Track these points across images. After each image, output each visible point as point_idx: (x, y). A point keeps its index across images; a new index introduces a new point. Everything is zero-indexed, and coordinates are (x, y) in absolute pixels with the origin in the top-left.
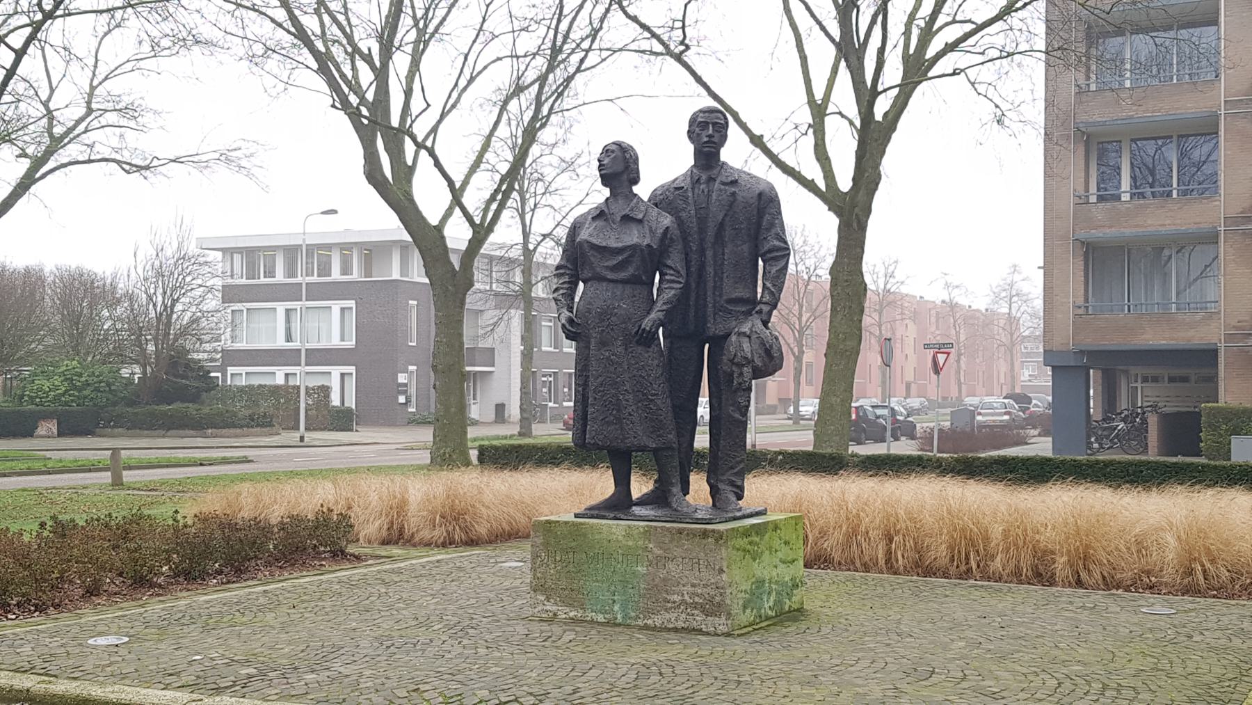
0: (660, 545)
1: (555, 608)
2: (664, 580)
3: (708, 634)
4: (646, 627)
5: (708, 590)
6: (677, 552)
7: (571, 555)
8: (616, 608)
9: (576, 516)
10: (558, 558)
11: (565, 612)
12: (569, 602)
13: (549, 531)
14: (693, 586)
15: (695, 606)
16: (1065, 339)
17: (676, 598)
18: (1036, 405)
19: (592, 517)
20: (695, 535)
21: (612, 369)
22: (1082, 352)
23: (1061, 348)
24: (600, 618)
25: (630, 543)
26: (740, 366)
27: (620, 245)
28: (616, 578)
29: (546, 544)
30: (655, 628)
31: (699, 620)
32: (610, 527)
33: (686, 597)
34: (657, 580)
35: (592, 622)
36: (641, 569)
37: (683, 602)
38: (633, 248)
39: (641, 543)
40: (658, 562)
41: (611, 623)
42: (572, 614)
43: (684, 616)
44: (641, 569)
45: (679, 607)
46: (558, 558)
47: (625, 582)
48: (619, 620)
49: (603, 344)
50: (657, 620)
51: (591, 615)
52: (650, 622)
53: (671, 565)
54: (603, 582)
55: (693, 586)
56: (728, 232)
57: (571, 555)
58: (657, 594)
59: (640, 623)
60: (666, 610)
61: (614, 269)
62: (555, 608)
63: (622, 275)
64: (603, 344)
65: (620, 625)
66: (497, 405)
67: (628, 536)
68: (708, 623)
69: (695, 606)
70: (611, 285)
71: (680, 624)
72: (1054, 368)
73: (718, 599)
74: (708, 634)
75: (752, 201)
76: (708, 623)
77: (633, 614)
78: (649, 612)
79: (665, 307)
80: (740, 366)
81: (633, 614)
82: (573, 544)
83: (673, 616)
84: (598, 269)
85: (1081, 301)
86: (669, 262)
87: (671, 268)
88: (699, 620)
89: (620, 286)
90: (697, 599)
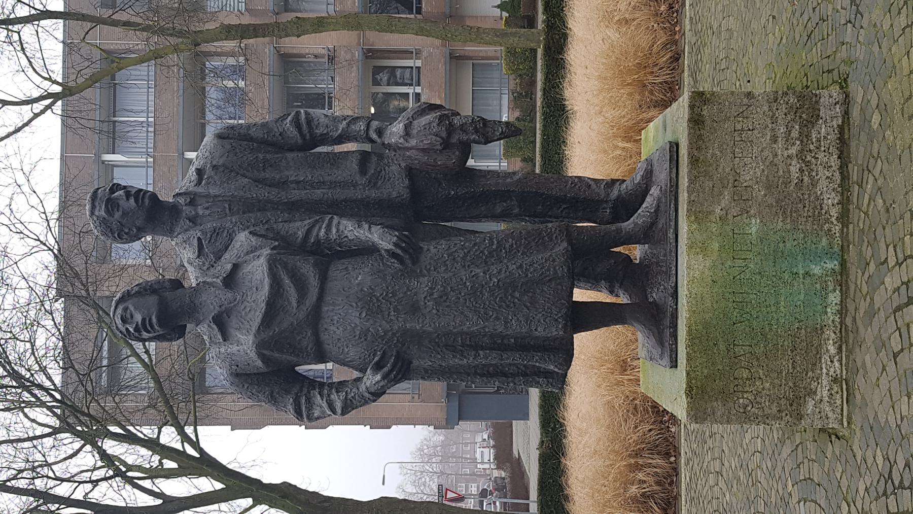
2: (769, 187)
3: (846, 114)
4: (844, 218)
5: (780, 114)
6: (725, 166)
8: (816, 270)
9: (674, 364)
10: (745, 374)
11: (830, 366)
12: (813, 356)
14: (774, 139)
15: (805, 137)
16: (438, 409)
17: (794, 169)
18: (489, 486)
19: (675, 336)
20: (700, 137)
21: (452, 296)
22: (448, 395)
23: (445, 414)
24: (834, 298)
25: (716, 246)
26: (451, 130)
27: (267, 282)
29: (725, 395)
30: (845, 203)
32: (691, 281)
33: (793, 151)
34: (771, 200)
35: (842, 311)
37: (800, 156)
38: (272, 265)
39: (714, 228)
40: (741, 198)
41: (842, 276)
42: (832, 350)
43: (821, 155)
44: (754, 227)
45: (808, 164)
49: (415, 309)
50: (831, 199)
51: (831, 316)
52: (834, 212)
53: (746, 177)
54: (778, 294)
55: (774, 139)
56: (269, 174)
59: (837, 228)
61: (302, 289)
63: (313, 282)
64: (415, 309)
65: (843, 264)
69: (805, 137)
70: (328, 298)
71: (834, 162)
72: (459, 419)
73: (792, 100)
74: (846, 114)
75: (228, 147)
77: (824, 241)
78: (818, 215)
79: (366, 226)
80: (451, 130)
81: (824, 241)
82: (722, 347)
83: (823, 174)
84: (301, 316)
85: (409, 397)
86: (300, 234)
87: (309, 232)
89: (330, 285)
90: (795, 134)
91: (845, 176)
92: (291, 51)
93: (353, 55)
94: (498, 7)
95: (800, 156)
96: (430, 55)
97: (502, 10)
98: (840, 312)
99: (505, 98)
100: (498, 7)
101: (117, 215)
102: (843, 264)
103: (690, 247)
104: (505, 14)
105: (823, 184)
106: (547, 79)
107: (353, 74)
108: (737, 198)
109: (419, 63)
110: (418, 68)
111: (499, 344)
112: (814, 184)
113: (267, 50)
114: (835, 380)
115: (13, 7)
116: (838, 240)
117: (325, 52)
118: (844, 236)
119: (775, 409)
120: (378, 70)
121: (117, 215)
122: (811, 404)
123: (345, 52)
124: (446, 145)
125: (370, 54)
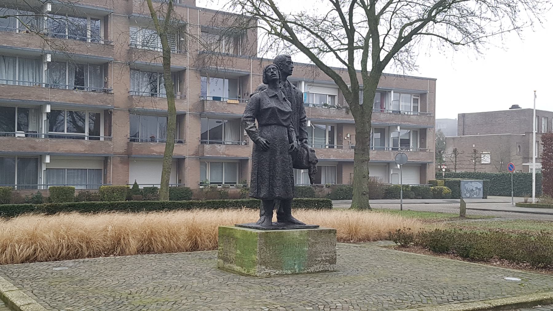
2: (315, 252)
4: (308, 273)
6: (320, 240)
10: (271, 248)
11: (273, 272)
17: (319, 259)
24: (289, 272)
29: (266, 242)
30: (312, 273)
31: (328, 266)
33: (323, 258)
37: (322, 260)
40: (313, 245)
42: (277, 273)
47: (299, 255)
48: (297, 271)
50: (312, 269)
53: (317, 245)
58: (312, 259)
59: (305, 271)
61: (285, 121)
65: (297, 274)
67: (301, 235)
71: (321, 269)
78: (310, 266)
83: (318, 266)
88: (328, 266)
90: (327, 258)
91: (318, 272)
92: (109, 69)
93: (109, 104)
94: (136, 183)
95: (322, 260)
96: (110, 146)
97: (134, 185)
98: (286, 274)
99: (83, 188)
100: (136, 183)
101: (287, 64)
102: (297, 274)
103: (301, 231)
104: (131, 187)
105: (316, 267)
106: (184, 204)
107: (98, 103)
108: (313, 243)
109: (102, 139)
110: (99, 139)
111: (272, 178)
112: (316, 264)
113: (111, 57)
114: (270, 274)
115: (340, 41)
116: (303, 272)
117: (109, 88)
118: (304, 273)
119: (262, 257)
120: (98, 116)
121: (287, 64)
122: (264, 267)
123: (110, 100)
124: (309, 163)
125: (108, 114)
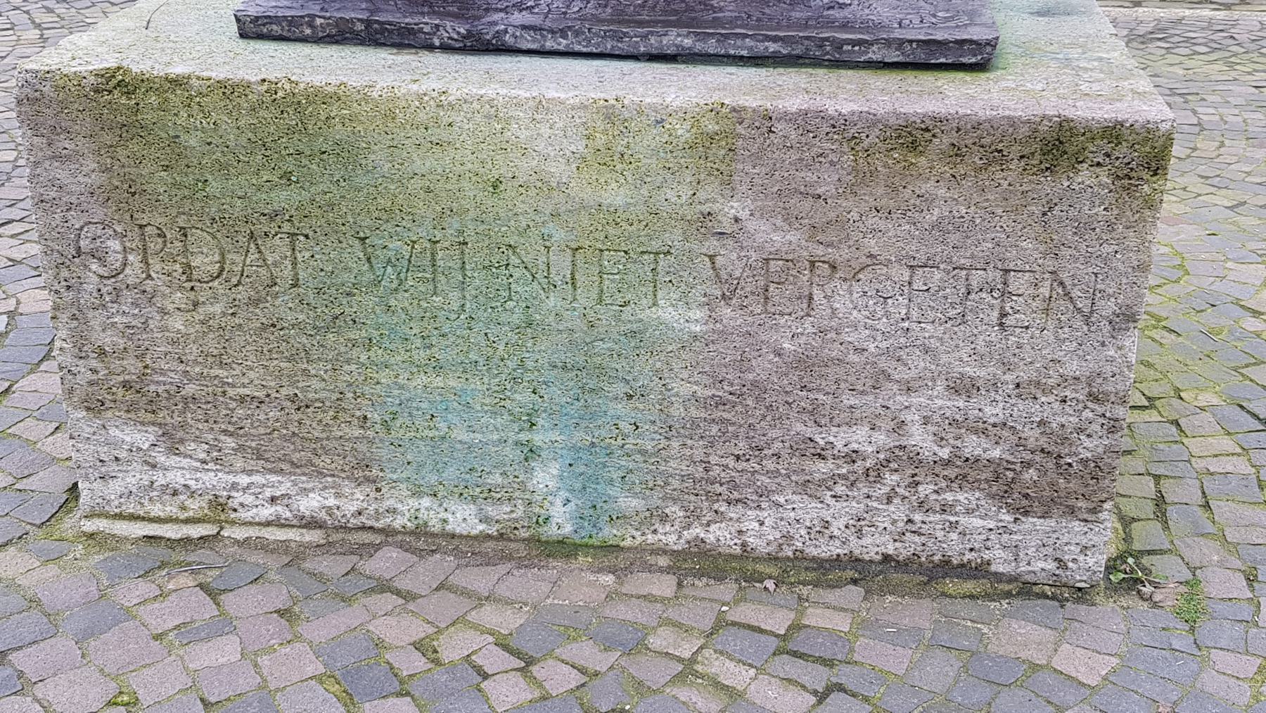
0: (785, 200)
1: (212, 479)
2: (804, 364)
3: (1025, 589)
5: (1047, 407)
6: (886, 237)
7: (277, 249)
9: (253, 29)
10: (205, 262)
11: (260, 497)
13: (131, 129)
15: (962, 471)
17: (859, 437)
20: (997, 157)
28: (543, 351)
31: (974, 526)
35: (422, 540)
36: (678, 315)
37: (901, 457)
42: (310, 504)
43: (898, 511)
46: (205, 262)
47: (587, 374)
50: (758, 529)
51: (406, 509)
52: (719, 535)
53: (844, 300)
55: (962, 387)
57: (277, 249)
59: (669, 537)
60: (805, 487)
62: (212, 479)
65: (564, 549)
66: (243, 35)
68: (1030, 545)
69: (962, 471)
71: (872, 546)
73: (1089, 447)
76: (1030, 545)
77: (630, 504)
78: (709, 492)
81: (630, 504)
83: (840, 514)
90: (973, 446)
